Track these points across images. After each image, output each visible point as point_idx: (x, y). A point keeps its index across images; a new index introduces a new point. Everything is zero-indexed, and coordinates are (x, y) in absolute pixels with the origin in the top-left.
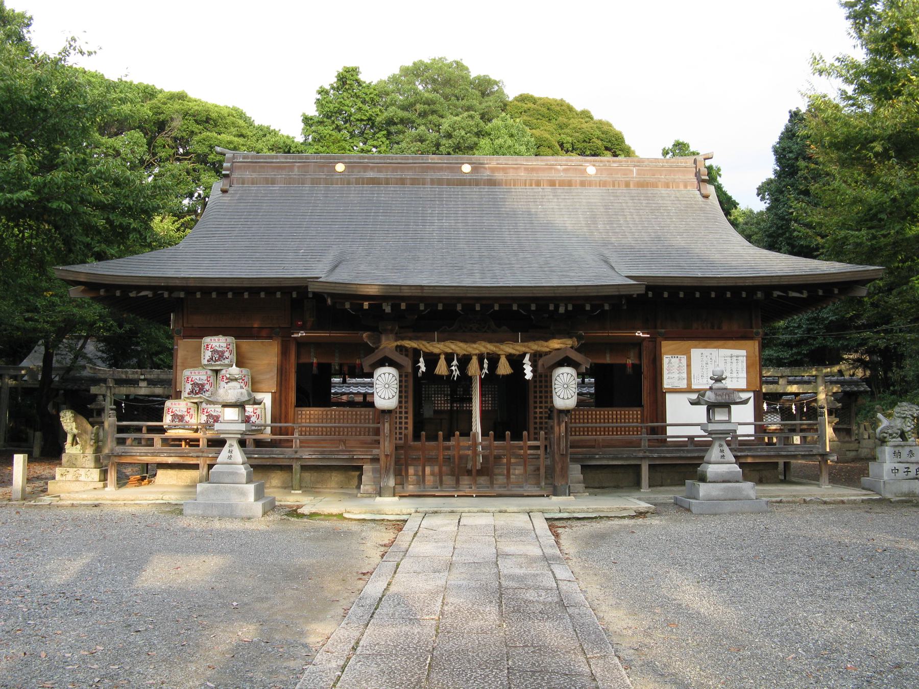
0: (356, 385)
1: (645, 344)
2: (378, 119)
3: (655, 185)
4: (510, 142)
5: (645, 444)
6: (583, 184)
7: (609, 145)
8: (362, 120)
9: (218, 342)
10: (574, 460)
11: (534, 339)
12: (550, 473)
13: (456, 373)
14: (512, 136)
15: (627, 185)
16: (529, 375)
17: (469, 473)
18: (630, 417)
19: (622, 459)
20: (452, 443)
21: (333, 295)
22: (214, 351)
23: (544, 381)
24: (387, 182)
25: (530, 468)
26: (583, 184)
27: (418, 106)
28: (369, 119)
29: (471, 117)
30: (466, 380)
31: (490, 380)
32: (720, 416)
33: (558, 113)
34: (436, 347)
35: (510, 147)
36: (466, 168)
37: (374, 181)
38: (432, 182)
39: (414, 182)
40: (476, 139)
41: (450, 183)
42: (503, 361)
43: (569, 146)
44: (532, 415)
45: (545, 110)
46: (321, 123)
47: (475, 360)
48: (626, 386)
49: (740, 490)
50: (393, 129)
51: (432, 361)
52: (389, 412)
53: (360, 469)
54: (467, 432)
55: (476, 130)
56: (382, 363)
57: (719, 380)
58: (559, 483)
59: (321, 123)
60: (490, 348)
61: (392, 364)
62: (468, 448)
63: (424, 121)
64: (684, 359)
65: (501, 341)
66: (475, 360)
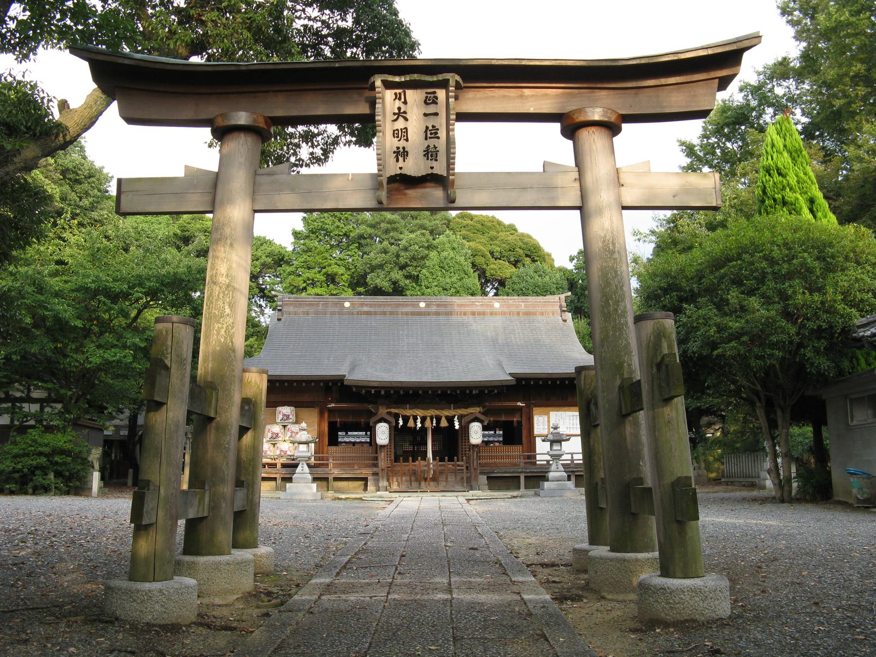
0: (354, 436)
1: (524, 409)
2: (352, 235)
3: (534, 314)
4: (452, 255)
5: (522, 465)
6: (491, 314)
7: (529, 253)
8: (339, 235)
9: (286, 410)
10: (482, 473)
11: (459, 408)
12: (469, 480)
13: (419, 425)
14: (454, 249)
15: (518, 314)
16: (457, 427)
17: (426, 479)
18: (516, 451)
19: (509, 473)
20: (417, 463)
21: (357, 387)
22: (284, 415)
23: (465, 429)
24: (375, 313)
25: (459, 478)
26: (491, 314)
27: (382, 225)
28: (345, 235)
29: (423, 234)
30: (424, 429)
31: (437, 430)
32: (556, 447)
33: (489, 228)
34: (408, 412)
35: (452, 258)
36: (422, 305)
37: (368, 313)
38: (402, 313)
39: (391, 313)
40: (426, 252)
41: (413, 314)
42: (443, 419)
43: (497, 255)
44: (460, 449)
45: (480, 226)
46: (307, 237)
47: (428, 419)
48: (516, 434)
49: (565, 485)
50: (362, 241)
51: (406, 419)
52: (384, 446)
53: (365, 480)
54: (424, 456)
55: (426, 245)
56: (380, 421)
57: (555, 428)
58: (474, 483)
59: (307, 237)
60: (437, 412)
61: (386, 421)
62: (425, 466)
63: (387, 236)
64: (546, 417)
65: (442, 409)
66: (428, 419)
